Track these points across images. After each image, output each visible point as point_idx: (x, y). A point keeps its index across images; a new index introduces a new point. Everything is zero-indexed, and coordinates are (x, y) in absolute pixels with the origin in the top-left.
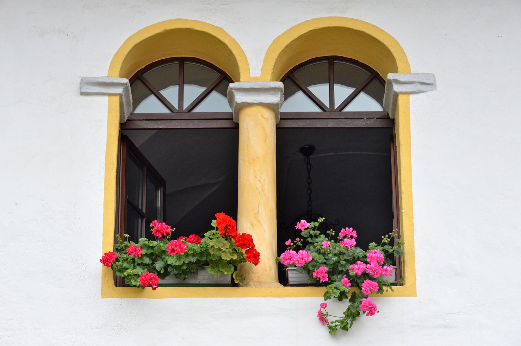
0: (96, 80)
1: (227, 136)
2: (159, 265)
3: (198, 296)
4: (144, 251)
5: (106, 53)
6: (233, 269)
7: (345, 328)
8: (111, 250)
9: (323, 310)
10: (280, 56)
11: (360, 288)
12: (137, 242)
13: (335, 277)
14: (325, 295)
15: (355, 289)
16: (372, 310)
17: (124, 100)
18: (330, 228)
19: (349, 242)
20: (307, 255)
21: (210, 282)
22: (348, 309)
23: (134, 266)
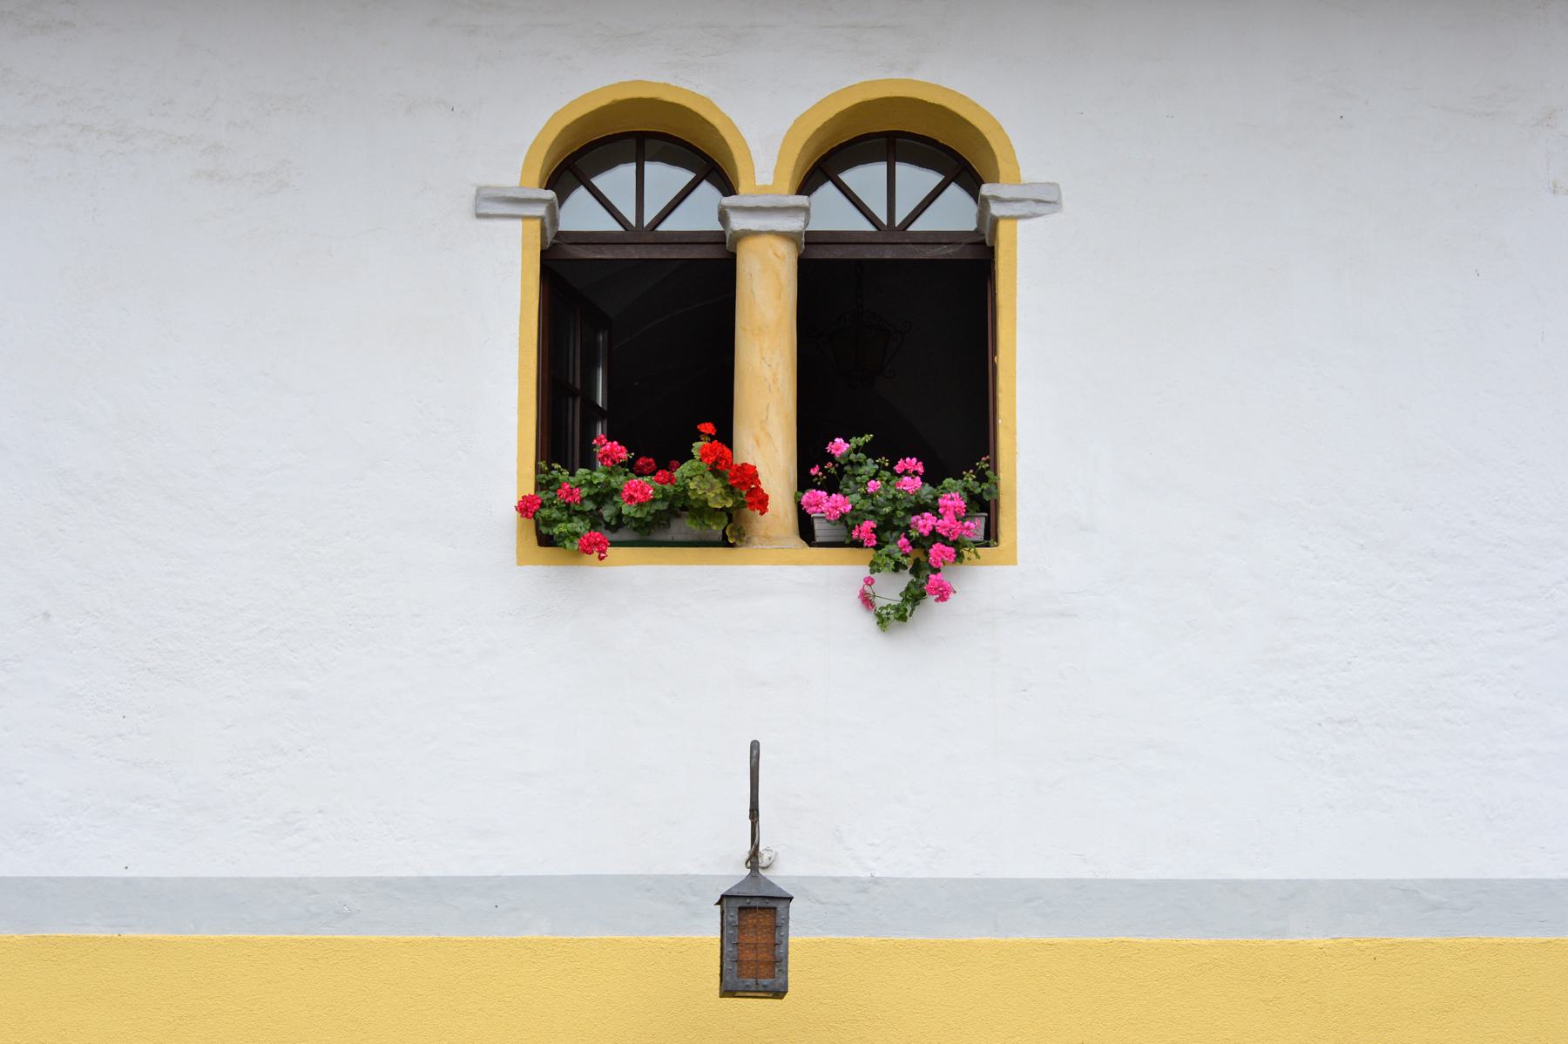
0: (502, 194)
2: (607, 512)
3: (671, 563)
4: (584, 491)
5: (515, 148)
6: (726, 520)
7: (903, 618)
9: (867, 588)
10: (805, 147)
11: (927, 554)
12: (572, 474)
13: (888, 534)
14: (872, 564)
16: (943, 594)
17: (547, 221)
19: (912, 485)
20: (839, 503)
21: (690, 538)
22: (908, 589)
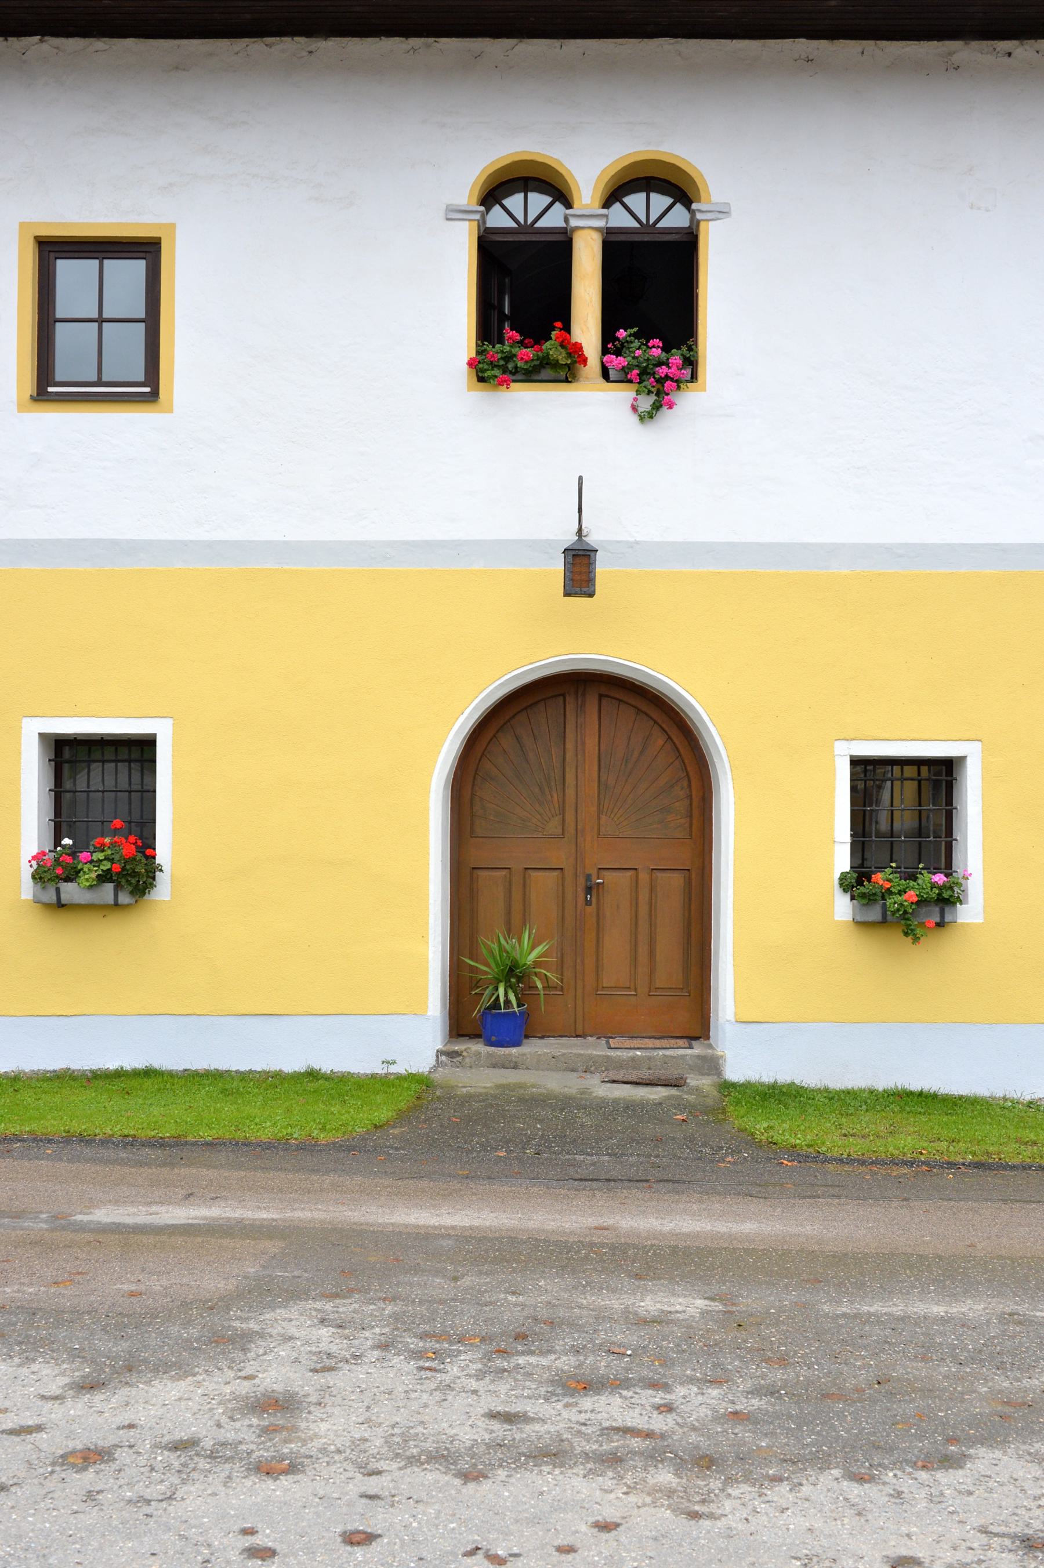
1: (560, 247)
5: (464, 184)
7: (651, 417)
8: (474, 355)
15: (659, 386)
18: (645, 335)
23: (491, 369)
